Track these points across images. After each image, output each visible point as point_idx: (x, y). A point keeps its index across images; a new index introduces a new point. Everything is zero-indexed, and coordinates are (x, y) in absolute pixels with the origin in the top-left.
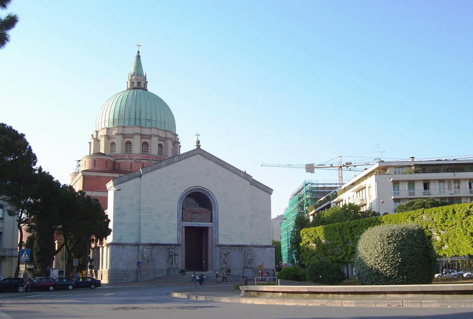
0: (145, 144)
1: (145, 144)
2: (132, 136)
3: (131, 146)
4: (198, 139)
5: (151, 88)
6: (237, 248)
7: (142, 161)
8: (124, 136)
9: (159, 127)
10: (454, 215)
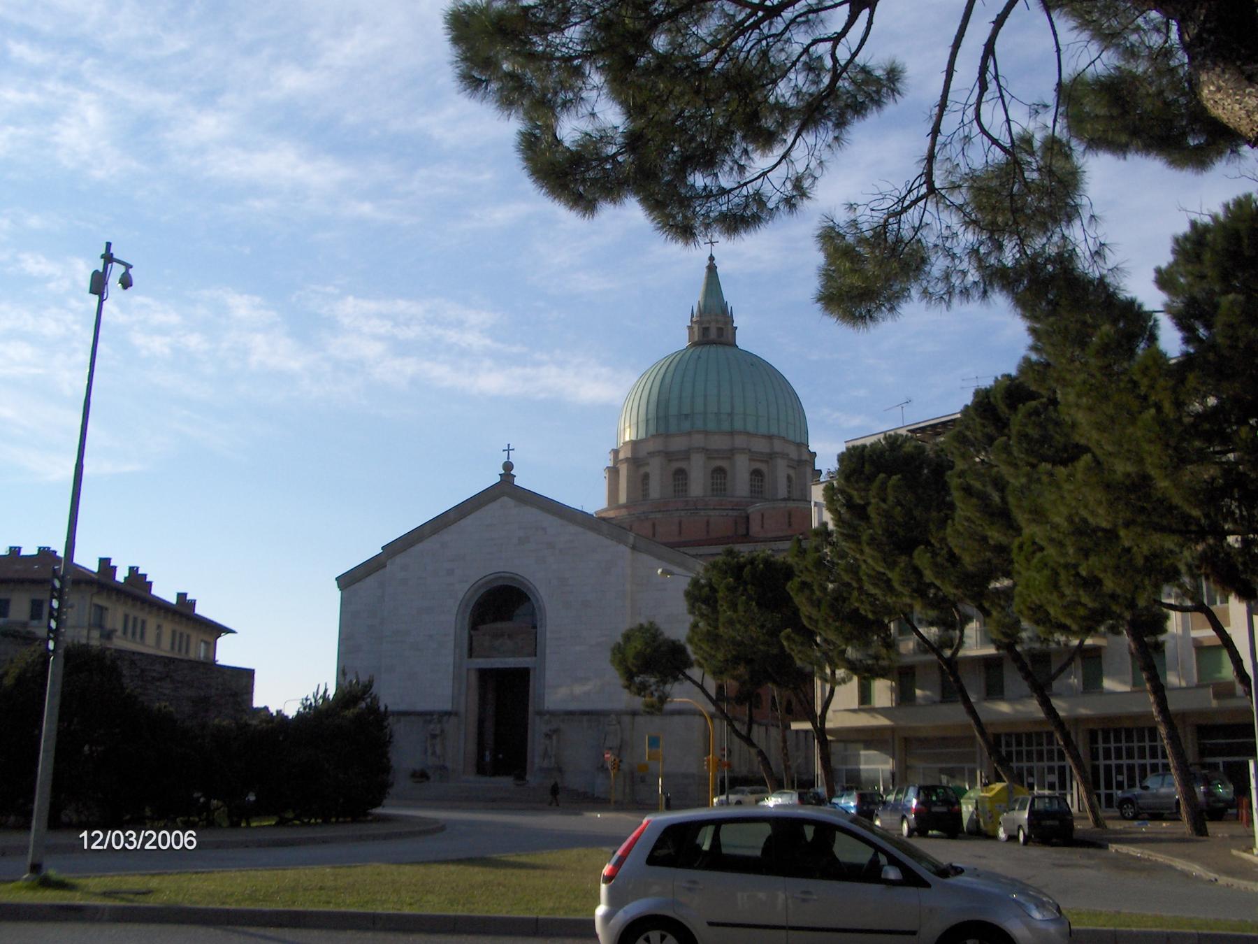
0: (719, 472)
1: (719, 472)
2: (686, 455)
3: (725, 478)
4: (508, 458)
5: (742, 341)
6: (585, 718)
7: (652, 516)
8: (669, 456)
9: (750, 428)
10: (74, 627)
